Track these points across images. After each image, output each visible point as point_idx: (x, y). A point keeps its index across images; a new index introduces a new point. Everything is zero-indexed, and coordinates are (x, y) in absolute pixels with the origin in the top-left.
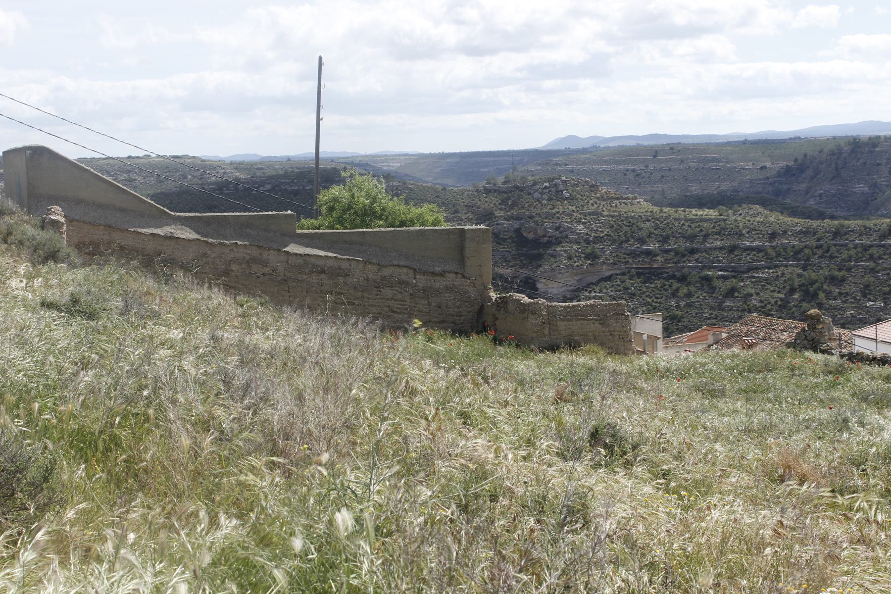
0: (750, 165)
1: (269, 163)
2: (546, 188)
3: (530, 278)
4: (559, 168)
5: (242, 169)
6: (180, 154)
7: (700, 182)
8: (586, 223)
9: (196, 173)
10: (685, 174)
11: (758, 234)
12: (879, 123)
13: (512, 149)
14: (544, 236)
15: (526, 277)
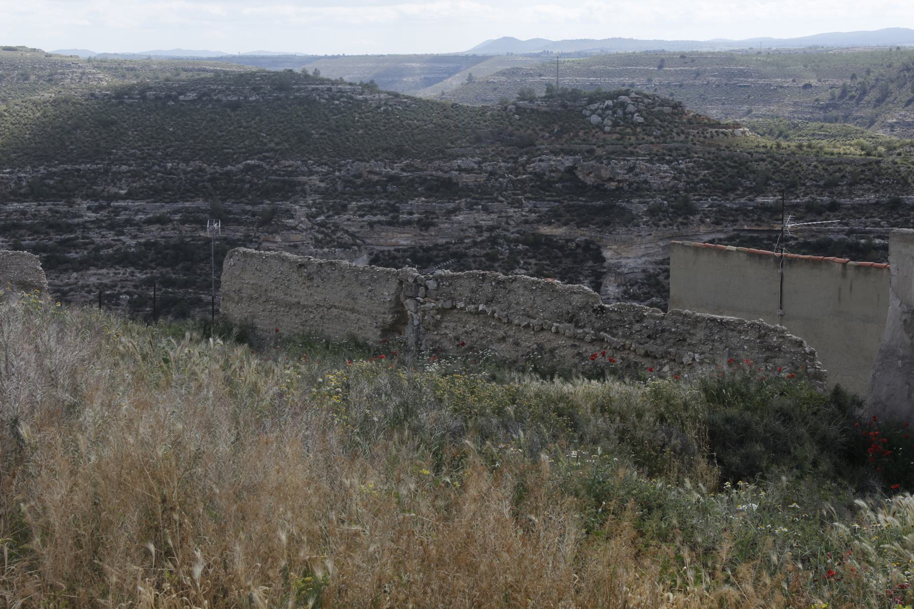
0: (789, 82)
1: (146, 63)
2: (608, 107)
3: (592, 242)
4: (531, 80)
5: (105, 68)
6: (14, 45)
7: (723, 104)
8: (672, 162)
10: (702, 92)
12: (697, 43)
14: (611, 179)
15: (586, 240)
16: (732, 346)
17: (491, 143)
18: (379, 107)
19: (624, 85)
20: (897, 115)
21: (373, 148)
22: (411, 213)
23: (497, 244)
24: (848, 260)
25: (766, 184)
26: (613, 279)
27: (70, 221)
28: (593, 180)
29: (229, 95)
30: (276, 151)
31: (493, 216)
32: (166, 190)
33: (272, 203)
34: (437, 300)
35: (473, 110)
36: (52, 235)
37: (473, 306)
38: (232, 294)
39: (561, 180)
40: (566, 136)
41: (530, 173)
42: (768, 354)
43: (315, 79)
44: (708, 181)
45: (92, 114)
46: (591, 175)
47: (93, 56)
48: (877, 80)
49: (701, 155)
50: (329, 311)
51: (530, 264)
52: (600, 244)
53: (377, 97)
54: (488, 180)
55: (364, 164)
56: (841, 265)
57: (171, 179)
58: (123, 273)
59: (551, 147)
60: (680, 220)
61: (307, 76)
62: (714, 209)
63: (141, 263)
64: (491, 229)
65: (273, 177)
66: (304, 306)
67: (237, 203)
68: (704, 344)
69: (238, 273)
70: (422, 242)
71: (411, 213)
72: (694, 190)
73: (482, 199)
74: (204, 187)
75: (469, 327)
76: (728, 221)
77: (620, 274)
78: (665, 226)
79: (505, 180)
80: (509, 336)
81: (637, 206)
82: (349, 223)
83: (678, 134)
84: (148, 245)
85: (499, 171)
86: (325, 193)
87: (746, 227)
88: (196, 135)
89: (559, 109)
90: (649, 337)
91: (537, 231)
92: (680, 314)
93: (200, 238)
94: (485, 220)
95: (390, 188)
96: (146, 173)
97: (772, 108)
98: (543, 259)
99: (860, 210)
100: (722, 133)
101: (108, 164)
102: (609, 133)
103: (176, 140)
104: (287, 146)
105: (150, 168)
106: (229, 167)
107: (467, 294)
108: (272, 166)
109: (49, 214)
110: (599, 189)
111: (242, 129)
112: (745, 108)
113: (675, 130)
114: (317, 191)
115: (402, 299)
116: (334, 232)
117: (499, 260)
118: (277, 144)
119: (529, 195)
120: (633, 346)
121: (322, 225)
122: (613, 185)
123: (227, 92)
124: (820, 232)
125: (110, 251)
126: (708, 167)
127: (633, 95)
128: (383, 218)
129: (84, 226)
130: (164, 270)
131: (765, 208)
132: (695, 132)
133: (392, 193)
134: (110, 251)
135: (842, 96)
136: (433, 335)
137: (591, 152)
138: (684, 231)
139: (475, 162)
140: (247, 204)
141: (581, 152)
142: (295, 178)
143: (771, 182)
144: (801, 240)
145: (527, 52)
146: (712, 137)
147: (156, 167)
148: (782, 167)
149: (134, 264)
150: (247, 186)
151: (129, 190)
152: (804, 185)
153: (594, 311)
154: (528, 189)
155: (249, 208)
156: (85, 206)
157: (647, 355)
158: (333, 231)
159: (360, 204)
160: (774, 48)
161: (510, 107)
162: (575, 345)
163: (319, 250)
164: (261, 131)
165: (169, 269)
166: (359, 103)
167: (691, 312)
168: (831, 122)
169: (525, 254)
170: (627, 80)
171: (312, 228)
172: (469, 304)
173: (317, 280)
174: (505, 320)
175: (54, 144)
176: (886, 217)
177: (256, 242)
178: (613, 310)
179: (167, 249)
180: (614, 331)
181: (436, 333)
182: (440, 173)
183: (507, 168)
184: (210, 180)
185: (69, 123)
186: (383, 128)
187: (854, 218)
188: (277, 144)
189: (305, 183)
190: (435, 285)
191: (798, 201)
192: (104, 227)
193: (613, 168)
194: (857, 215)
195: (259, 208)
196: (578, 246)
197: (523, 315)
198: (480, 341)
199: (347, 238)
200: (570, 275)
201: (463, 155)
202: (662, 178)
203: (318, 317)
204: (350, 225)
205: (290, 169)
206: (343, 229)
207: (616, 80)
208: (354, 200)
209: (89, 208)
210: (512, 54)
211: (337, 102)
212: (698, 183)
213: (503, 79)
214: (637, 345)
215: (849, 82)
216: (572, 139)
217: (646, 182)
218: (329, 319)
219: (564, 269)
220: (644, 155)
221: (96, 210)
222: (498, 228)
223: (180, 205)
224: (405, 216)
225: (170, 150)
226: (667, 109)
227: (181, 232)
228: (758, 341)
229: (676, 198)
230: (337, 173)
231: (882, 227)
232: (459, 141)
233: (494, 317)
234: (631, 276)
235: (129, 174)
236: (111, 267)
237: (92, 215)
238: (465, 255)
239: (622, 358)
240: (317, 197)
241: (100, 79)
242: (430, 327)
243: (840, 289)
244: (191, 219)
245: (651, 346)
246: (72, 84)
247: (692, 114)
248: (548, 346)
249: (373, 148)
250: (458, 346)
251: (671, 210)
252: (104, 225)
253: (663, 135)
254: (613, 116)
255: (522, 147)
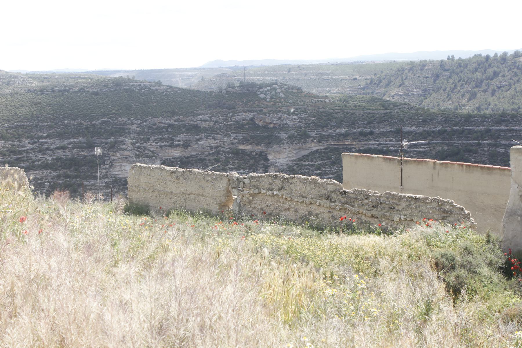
1: (53, 75)
2: (268, 90)
3: (263, 152)
4: (230, 79)
5: (34, 78)
7: (318, 88)
8: (298, 114)
9: (4, 81)
11: (414, 122)
13: (183, 67)
14: (270, 123)
15: (260, 152)
16: (423, 211)
17: (215, 108)
18: (163, 93)
19: (273, 80)
20: (395, 91)
21: (161, 112)
22: (179, 141)
23: (220, 154)
24: (436, 160)
25: (340, 123)
26: (273, 169)
27: (20, 149)
28: (262, 123)
29: (93, 89)
30: (116, 114)
31: (218, 141)
32: (65, 133)
33: (115, 138)
34: (250, 189)
35: (206, 93)
36: (12, 156)
37: (271, 192)
38: (134, 188)
39: (248, 124)
40: (249, 104)
41: (234, 121)
42: (444, 215)
43: (133, 81)
44: (314, 123)
45: (29, 99)
46: (262, 121)
47: (28, 72)
48: (386, 76)
49: (311, 111)
50: (189, 196)
51: (235, 163)
52: (267, 153)
53: (162, 88)
54: (214, 125)
55: (157, 119)
56: (433, 163)
57: (67, 128)
58: (46, 172)
59: (242, 109)
60: (303, 141)
61: (129, 79)
62: (318, 135)
63: (54, 168)
64: (216, 147)
65: (115, 126)
66: (175, 194)
67: (98, 139)
68: (406, 210)
69: (137, 177)
70: (185, 154)
71: (179, 141)
72: (308, 127)
73: (212, 134)
74: (83, 131)
75: (268, 203)
76: (324, 141)
77: (276, 166)
78: (296, 144)
79: (222, 125)
80: (292, 208)
81: (283, 135)
82: (151, 146)
83: (300, 102)
84: (57, 159)
85: (219, 121)
86: (139, 133)
87: (332, 143)
88: (78, 107)
89: (246, 91)
90: (373, 207)
91: (237, 148)
92: (390, 194)
93: (82, 155)
94: (214, 143)
95: (169, 130)
96: (55, 126)
97: (340, 89)
98: (241, 160)
99: (383, 134)
100: (320, 101)
101: (38, 122)
102: (269, 102)
103: (69, 110)
104: (121, 112)
105: (57, 123)
106: (94, 122)
107: (267, 185)
108: (114, 121)
109: (10, 146)
110: (265, 128)
111: (100, 104)
112: (328, 89)
113: (299, 100)
114: (135, 132)
115: (230, 188)
116: (144, 151)
117: (220, 161)
118: (116, 111)
119: (233, 131)
120: (364, 212)
121: (139, 147)
122: (272, 126)
123: (92, 88)
124: (366, 145)
125: (40, 163)
126: (315, 117)
127: (279, 84)
128: (167, 144)
129: (27, 151)
130: (65, 171)
131: (340, 135)
132: (308, 100)
133: (170, 132)
134: (40, 163)
135: (371, 83)
136: (248, 208)
137: (261, 111)
138: (304, 146)
139: (208, 117)
140: (103, 139)
141: (256, 111)
142: (125, 127)
143: (343, 122)
144: (357, 148)
145: (227, 66)
146: (316, 103)
147: (60, 123)
148: (348, 116)
149: (51, 168)
150: (103, 130)
151: (48, 134)
152: (358, 123)
153: (341, 193)
154: (233, 128)
155: (104, 141)
156: (27, 142)
157: (372, 216)
158: (143, 150)
159: (155, 137)
160: (339, 63)
161: (223, 91)
162: (330, 212)
163: (137, 159)
164: (108, 105)
165: (67, 170)
166: (153, 92)
167: (396, 193)
168: (366, 95)
169: (233, 158)
170: (274, 78)
171: (133, 150)
172: (269, 191)
173: (182, 180)
174: (290, 199)
175: (11, 113)
176: (395, 137)
177: (108, 156)
178: (351, 193)
179: (66, 161)
180: (353, 204)
181: (249, 206)
182: (192, 122)
183: (223, 119)
184: (85, 128)
185: (19, 103)
186: (165, 102)
187: (381, 138)
188: (116, 111)
189: (130, 129)
190: (249, 181)
191: (355, 131)
192: (36, 152)
193: (271, 118)
194: (382, 137)
195: (109, 141)
196: (256, 154)
197: (300, 196)
198: (275, 210)
199: (150, 153)
200: (253, 167)
201: (203, 114)
202: (294, 122)
203: (183, 200)
204: (151, 147)
205: (123, 122)
206: (148, 149)
207: (269, 78)
208: (153, 136)
209: (29, 143)
210: (221, 67)
211: (143, 91)
212: (310, 124)
213: (218, 78)
214: (366, 211)
215: (373, 77)
216: (252, 105)
217: (286, 124)
218: (189, 200)
219: (250, 165)
220: (285, 112)
221: (33, 144)
222: (220, 147)
223: (72, 140)
224: (177, 142)
225: (66, 115)
226: (295, 91)
227: (72, 153)
228: (438, 208)
229: (300, 131)
230: (145, 124)
231: (393, 142)
232: (201, 107)
233: (283, 198)
234: (281, 167)
235: (47, 127)
236: (40, 170)
237: (30, 146)
238: (205, 159)
239: (358, 218)
240: (136, 135)
241: (31, 83)
242: (247, 204)
243: (432, 175)
244: (77, 146)
245: (375, 212)
246: (18, 85)
247: (306, 93)
248: (314, 213)
249: (161, 112)
250: (262, 213)
251: (298, 136)
252: (36, 150)
253: (293, 103)
254: (270, 94)
255: (230, 110)
